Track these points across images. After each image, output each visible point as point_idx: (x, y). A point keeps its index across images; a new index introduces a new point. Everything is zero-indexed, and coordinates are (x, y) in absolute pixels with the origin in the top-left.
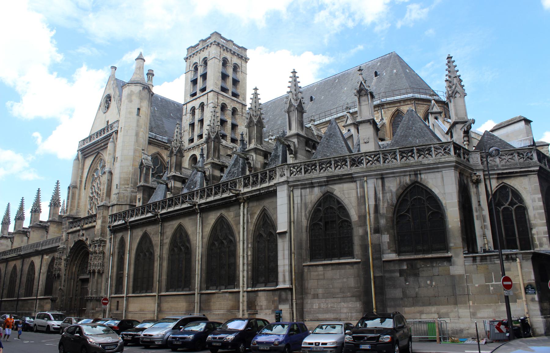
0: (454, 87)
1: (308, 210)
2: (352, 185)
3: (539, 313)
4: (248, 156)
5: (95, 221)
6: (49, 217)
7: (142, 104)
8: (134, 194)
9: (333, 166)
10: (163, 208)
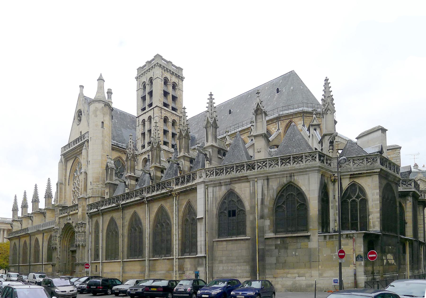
0: (327, 105)
1: (217, 202)
2: (247, 184)
3: (363, 273)
4: (178, 162)
5: (77, 209)
6: (45, 206)
8: (103, 189)
10: (123, 200)
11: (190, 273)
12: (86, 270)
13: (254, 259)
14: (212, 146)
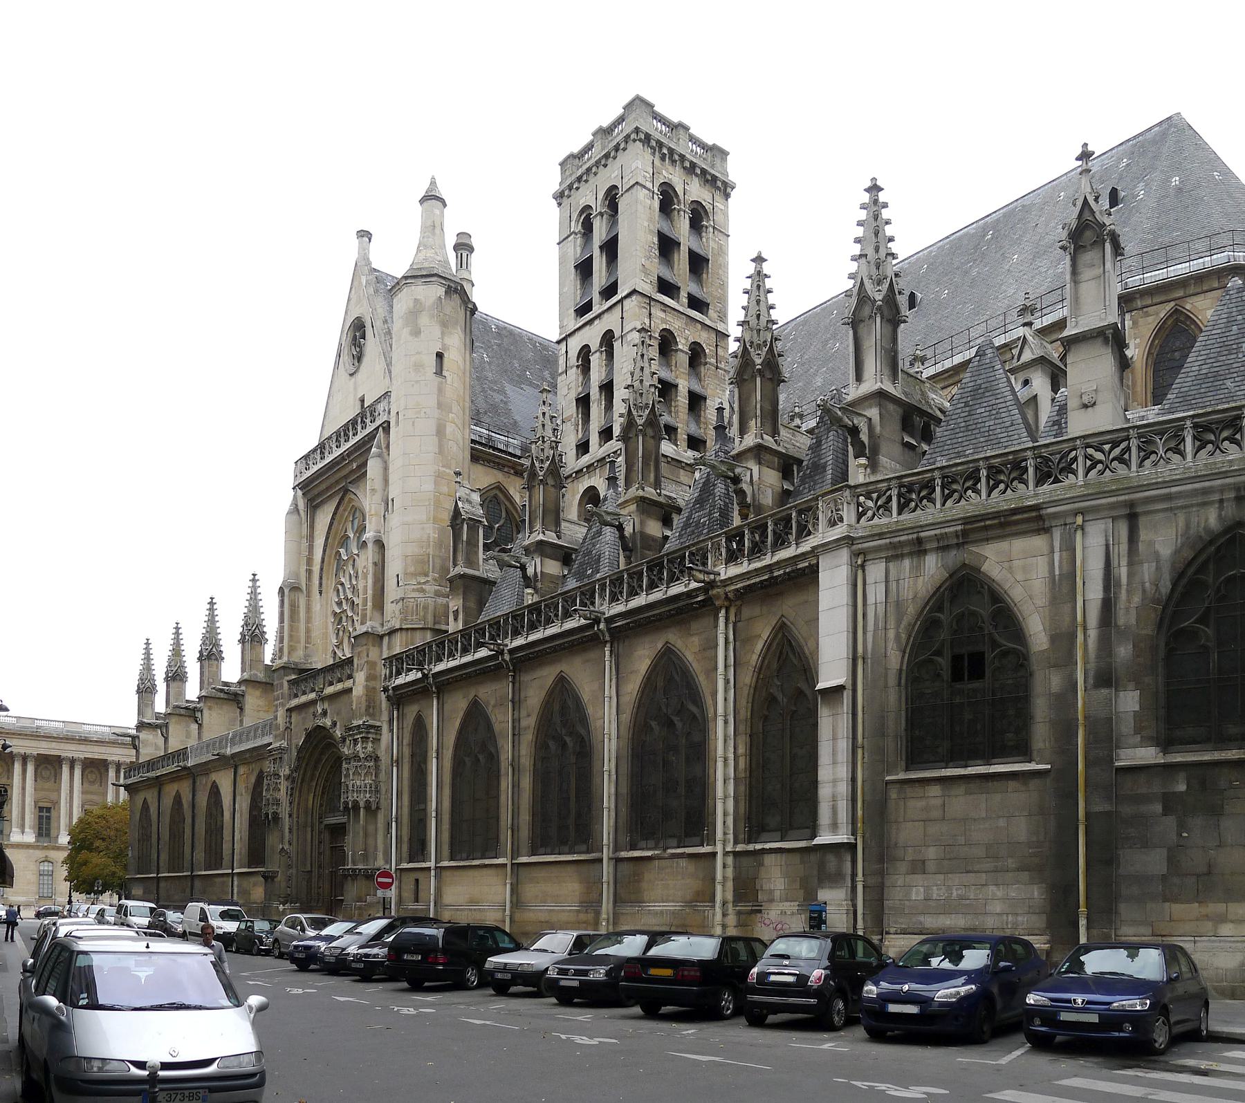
4: (738, 470)
5: (350, 677)
6: (243, 670)
7: (448, 341)
8: (441, 600)
9: (982, 486)
10: (516, 633)
11: (783, 913)
12: (380, 893)
13: (1066, 857)
14: (881, 395)
